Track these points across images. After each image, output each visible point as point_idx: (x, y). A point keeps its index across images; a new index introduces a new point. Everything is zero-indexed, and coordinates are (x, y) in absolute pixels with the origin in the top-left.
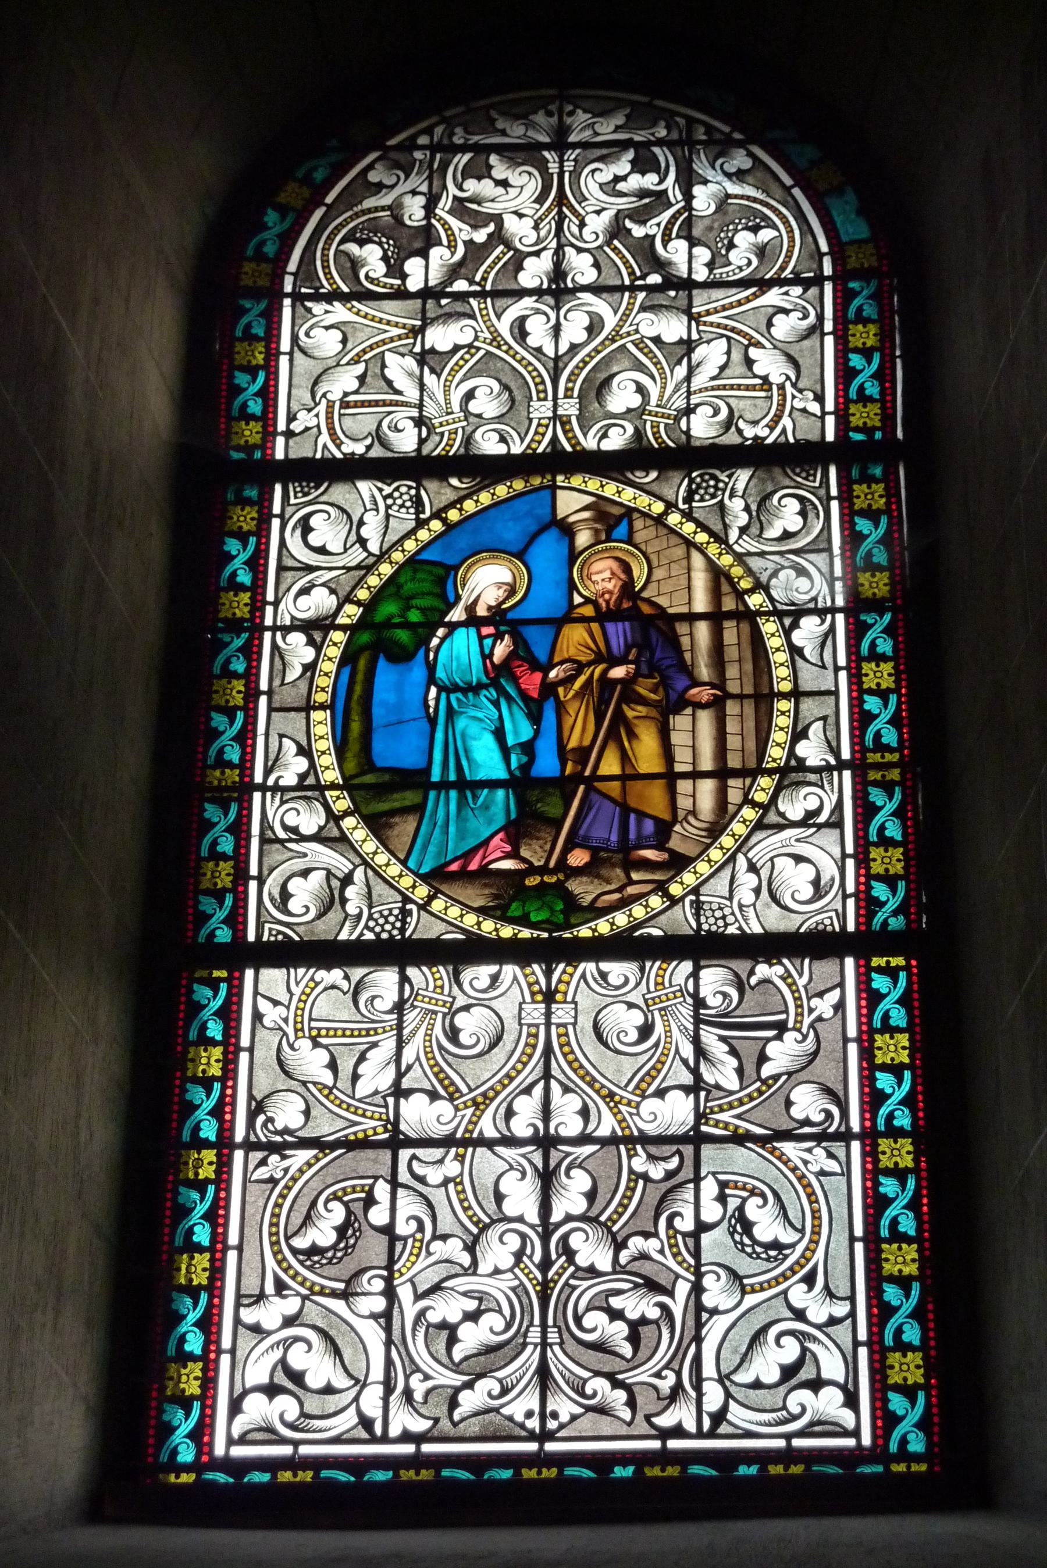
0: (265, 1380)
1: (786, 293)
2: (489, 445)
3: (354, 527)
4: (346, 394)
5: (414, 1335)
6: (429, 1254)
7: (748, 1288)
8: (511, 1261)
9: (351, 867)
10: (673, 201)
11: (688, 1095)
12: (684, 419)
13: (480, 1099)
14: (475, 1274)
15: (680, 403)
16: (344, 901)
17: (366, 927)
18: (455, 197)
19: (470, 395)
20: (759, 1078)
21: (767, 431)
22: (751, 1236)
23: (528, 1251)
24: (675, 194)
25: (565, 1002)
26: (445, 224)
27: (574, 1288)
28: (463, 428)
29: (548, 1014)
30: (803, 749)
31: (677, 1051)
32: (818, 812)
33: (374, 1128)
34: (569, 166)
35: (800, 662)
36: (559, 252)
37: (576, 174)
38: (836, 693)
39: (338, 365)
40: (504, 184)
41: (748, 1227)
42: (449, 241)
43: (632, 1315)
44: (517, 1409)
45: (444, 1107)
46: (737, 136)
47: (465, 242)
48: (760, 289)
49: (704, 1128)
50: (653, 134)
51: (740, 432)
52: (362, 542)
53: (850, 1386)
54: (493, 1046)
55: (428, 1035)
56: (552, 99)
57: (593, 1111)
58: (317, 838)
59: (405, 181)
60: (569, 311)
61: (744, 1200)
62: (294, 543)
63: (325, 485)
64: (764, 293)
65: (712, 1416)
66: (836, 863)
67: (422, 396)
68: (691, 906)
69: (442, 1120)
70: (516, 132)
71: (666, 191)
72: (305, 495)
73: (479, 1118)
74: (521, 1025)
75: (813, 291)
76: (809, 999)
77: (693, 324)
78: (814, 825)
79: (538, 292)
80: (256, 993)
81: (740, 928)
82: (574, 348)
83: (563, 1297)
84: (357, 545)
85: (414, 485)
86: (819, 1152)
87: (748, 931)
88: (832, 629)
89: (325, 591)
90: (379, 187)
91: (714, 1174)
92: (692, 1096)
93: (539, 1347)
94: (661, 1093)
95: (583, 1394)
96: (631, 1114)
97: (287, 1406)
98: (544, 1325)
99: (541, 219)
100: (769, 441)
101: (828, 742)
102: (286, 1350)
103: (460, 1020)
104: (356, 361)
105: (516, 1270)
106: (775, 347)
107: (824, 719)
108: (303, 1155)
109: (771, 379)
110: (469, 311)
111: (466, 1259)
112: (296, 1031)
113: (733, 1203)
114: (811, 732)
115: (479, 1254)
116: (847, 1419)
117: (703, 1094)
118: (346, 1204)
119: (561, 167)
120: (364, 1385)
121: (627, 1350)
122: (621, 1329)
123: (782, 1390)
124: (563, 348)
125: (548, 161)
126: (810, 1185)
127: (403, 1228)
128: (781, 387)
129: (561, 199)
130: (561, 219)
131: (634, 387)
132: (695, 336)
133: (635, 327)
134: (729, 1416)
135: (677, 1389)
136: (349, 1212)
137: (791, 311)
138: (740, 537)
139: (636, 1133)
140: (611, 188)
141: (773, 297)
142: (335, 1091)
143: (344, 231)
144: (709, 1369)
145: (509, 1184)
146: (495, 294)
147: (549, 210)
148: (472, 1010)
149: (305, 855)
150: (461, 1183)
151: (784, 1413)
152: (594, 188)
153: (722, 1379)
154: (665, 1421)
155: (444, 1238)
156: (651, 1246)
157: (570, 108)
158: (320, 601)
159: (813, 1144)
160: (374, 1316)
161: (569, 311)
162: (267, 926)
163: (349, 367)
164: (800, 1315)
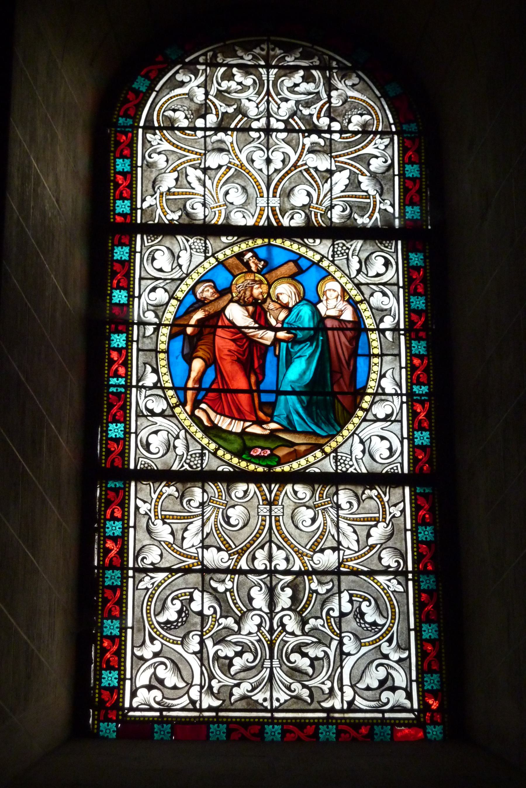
0: (147, 683)
5: (214, 667)
6: (219, 625)
7: (363, 644)
9: (357, 277)
11: (334, 552)
12: (329, 212)
13: (240, 551)
14: (240, 634)
15: (327, 203)
17: (349, 249)
19: (227, 193)
20: (178, 171)
21: (368, 220)
22: (364, 620)
23: (263, 625)
24: (324, 96)
26: (213, 103)
28: (316, 501)
29: (270, 510)
31: (329, 531)
32: (392, 414)
33: (193, 563)
34: (272, 78)
39: (382, 544)
41: (362, 615)
44: (259, 697)
45: (224, 555)
49: (342, 569)
52: (362, 442)
53: (409, 689)
54: (245, 525)
56: (263, 42)
57: (291, 558)
58: (162, 414)
59: (195, 79)
60: (273, 151)
61: (361, 603)
67: (205, 191)
69: (223, 560)
70: (247, 60)
74: (259, 515)
76: (389, 508)
77: (201, 559)
78: (390, 421)
80: (136, 497)
81: (355, 469)
83: (281, 647)
86: (395, 582)
87: (360, 471)
90: (182, 84)
91: (347, 591)
94: (322, 551)
97: (157, 694)
99: (260, 103)
100: (369, 226)
102: (155, 669)
103: (230, 512)
105: (258, 633)
107: (144, 337)
108: (160, 576)
111: (236, 627)
112: (155, 516)
113: (356, 605)
114: (387, 375)
115: (241, 625)
118: (181, 601)
119: (268, 77)
120: (191, 686)
121: (310, 671)
122: (307, 661)
123: (379, 691)
125: (261, 74)
126: (390, 596)
128: (374, 197)
130: (268, 102)
131: (306, 193)
134: (356, 702)
135: (331, 689)
136: (183, 606)
139: (310, 569)
142: (174, 545)
144: (346, 681)
145: (255, 592)
148: (236, 507)
150: (233, 592)
154: (327, 705)
157: (273, 46)
158: (161, 296)
159: (392, 577)
160: (195, 653)
161: (273, 151)
162: (393, 250)
164: (386, 657)
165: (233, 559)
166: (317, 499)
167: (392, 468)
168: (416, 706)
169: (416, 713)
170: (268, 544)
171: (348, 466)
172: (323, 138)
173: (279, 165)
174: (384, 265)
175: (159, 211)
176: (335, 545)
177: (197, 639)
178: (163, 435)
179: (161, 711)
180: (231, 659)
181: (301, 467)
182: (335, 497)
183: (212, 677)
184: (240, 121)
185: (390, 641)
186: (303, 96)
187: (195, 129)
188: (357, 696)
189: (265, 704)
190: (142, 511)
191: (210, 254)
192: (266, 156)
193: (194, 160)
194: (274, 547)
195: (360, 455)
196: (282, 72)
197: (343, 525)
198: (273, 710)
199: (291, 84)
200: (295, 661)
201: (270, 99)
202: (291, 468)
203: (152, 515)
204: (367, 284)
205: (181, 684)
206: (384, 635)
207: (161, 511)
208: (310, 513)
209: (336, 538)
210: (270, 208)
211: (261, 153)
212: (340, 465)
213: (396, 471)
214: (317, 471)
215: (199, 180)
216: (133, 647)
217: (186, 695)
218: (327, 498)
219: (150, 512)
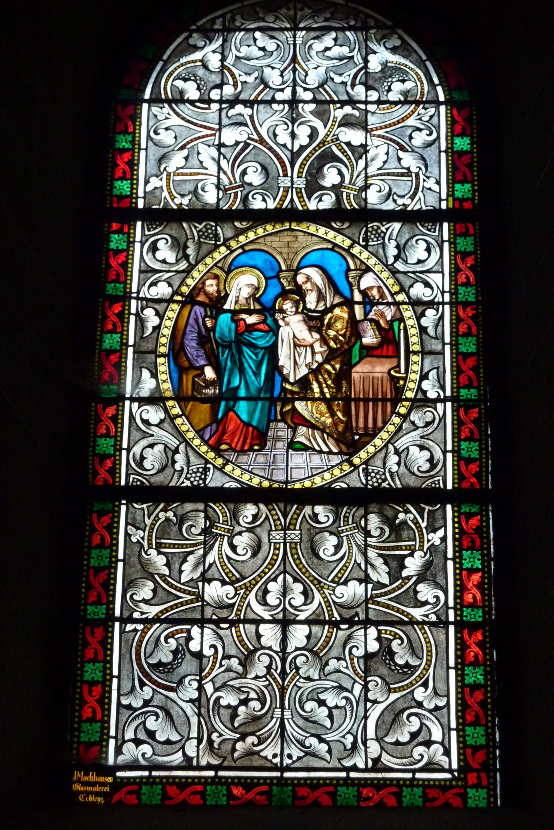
1: (143, 613)
2: (257, 204)
3: (403, 461)
4: (178, 169)
8: (265, 671)
9: (178, 443)
11: (360, 584)
12: (364, 193)
13: (248, 585)
15: (360, 182)
16: (398, 247)
21: (410, 200)
23: (274, 667)
24: (358, 59)
25: (295, 529)
27: (300, 688)
28: (241, 191)
35: (424, 337)
38: (442, 353)
39: (173, 150)
42: (234, 82)
43: (331, 704)
48: (159, 617)
50: (347, 23)
51: (395, 201)
55: (352, 175)
61: (391, 641)
63: (165, 223)
64: (157, 615)
65: (373, 760)
66: (441, 449)
72: (154, 229)
73: (248, 595)
77: (368, 134)
81: (389, 484)
82: (302, 148)
88: (442, 317)
89: (165, 284)
90: (196, 48)
92: (364, 584)
95: (304, 746)
96: (330, 594)
98: (295, 45)
104: (182, 148)
105: (268, 676)
107: (438, 368)
109: (411, 169)
111: (240, 669)
117: (370, 586)
121: (328, 724)
122: (323, 712)
124: (280, 579)
130: (294, 70)
134: (382, 760)
135: (355, 744)
137: (423, 129)
138: (178, 446)
144: (371, 733)
147: (289, 65)
148: (243, 534)
149: (152, 435)
151: (411, 759)
153: (378, 739)
154: (348, 763)
156: (244, 78)
160: (191, 701)
165: (239, 594)
167: (434, 482)
168: (455, 766)
169: (456, 774)
172: (359, 109)
173: (272, 586)
175: (424, 525)
176: (362, 576)
177: (195, 684)
180: (236, 708)
181: (324, 482)
183: (212, 730)
184: (261, 92)
185: (425, 685)
186: (335, 61)
187: (209, 101)
188: (383, 752)
190: (433, 180)
191: (361, 469)
193: (207, 136)
194: (289, 579)
195: (395, 468)
196: (313, 34)
197: (372, 553)
200: (287, 324)
202: (313, 483)
203: (146, 544)
204: (405, 273)
205: (175, 737)
207: (412, 181)
210: (294, 190)
211: (294, 603)
212: (371, 480)
213: (437, 486)
214: (344, 486)
215: (372, 566)
216: (119, 695)
217: (181, 751)
218: (230, 194)
219: (143, 540)
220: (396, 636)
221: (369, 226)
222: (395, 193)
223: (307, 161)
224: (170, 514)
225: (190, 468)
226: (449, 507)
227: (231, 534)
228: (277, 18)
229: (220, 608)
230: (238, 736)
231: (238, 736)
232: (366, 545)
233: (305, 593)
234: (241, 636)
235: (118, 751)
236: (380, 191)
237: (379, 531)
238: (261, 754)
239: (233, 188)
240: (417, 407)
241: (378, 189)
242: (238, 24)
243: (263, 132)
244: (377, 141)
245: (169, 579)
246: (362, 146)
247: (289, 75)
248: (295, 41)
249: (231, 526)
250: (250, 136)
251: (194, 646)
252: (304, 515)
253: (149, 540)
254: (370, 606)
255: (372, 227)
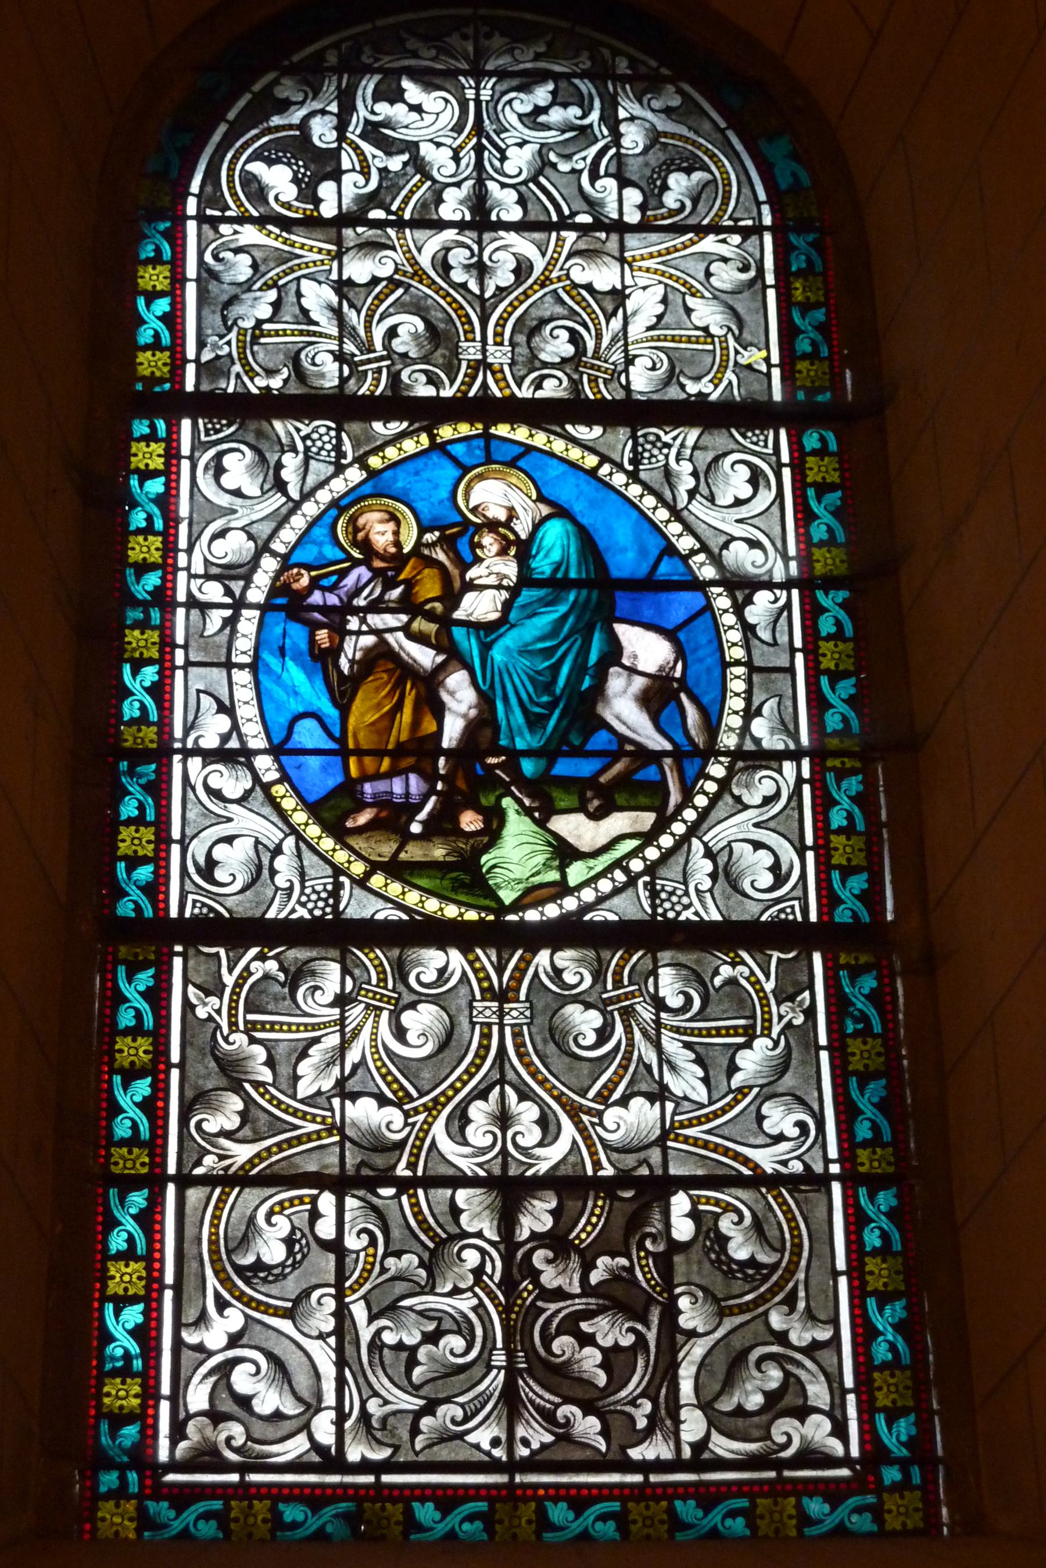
1: (724, 241)
3: (271, 472)
9: (690, 507)
10: (600, 137)
11: (652, 1104)
14: (432, 1292)
15: (355, 1012)
16: (273, 872)
17: (299, 902)
18: (367, 122)
20: (280, 289)
21: (711, 387)
28: (388, 367)
30: (759, 727)
34: (486, 94)
36: (480, 183)
37: (495, 100)
38: (791, 670)
39: (762, 1086)
40: (417, 109)
42: (362, 167)
44: (483, 1437)
46: (664, 71)
47: (380, 170)
51: (682, 387)
52: (709, 854)
53: (838, 1414)
62: (206, 483)
64: (701, 239)
66: (199, 490)
68: (645, 888)
71: (591, 126)
75: (754, 239)
79: (461, 226)
81: (696, 913)
84: (715, 850)
85: (333, 425)
87: (706, 918)
88: (788, 606)
92: (658, 1104)
93: (503, 1372)
96: (593, 1124)
100: (714, 397)
101: (783, 722)
105: (477, 1289)
106: (715, 297)
110: (615, 1156)
116: (837, 1447)
117: (670, 1106)
123: (765, 1418)
127: (352, 1242)
128: (233, 1025)
129: (479, 129)
132: (336, 1102)
133: (410, 1120)
134: (711, 1445)
140: (533, 118)
141: (709, 244)
143: (250, 151)
146: (416, 224)
151: (769, 1443)
152: (513, 119)
153: (705, 1406)
155: (398, 1254)
157: (486, 29)
162: (191, 897)
163: (751, 1082)
165: (414, 1124)
166: (609, 987)
167: (782, 910)
168: (855, 1452)
170: (498, 1088)
171: (678, 908)
174: (748, 481)
175: (769, 986)
176: (655, 1088)
177: (331, 1304)
178: (243, 848)
179: (242, 1469)
180: (413, 1350)
182: (651, 980)
185: (790, 1301)
189: (498, 1453)
192: (510, 1134)
195: (707, 883)
197: (671, 1045)
198: (513, 1466)
199: (528, 108)
201: (484, 141)
205: (291, 1408)
206: (712, 1146)
207: (714, 351)
208: (594, 1019)
209: (657, 1077)
213: (791, 917)
215: (673, 1068)
218: (366, 372)
220: (728, 1208)
221: (639, 433)
222: (283, 985)
223: (472, 1063)
224: (272, 966)
225: (307, 884)
226: (817, 958)
227: (395, 1005)
228: (441, 51)
229: (375, 1149)
230: (422, 1402)
231: (422, 1402)
232: (658, 1023)
233: (544, 1122)
234: (421, 1212)
235: (178, 1432)
236: (653, 368)
237: (318, 361)
238: (466, 1438)
239: (627, 996)
240: (241, 566)
241: (650, 365)
242: (365, 59)
243: (425, 260)
244: (643, 280)
245: (683, 289)
246: (614, 291)
247: (468, 158)
248: (478, 94)
249: (394, 991)
250: (596, 1120)
251: (326, 1229)
252: (536, 974)
253: (230, 1015)
254: (670, 1144)
255: (645, 436)
